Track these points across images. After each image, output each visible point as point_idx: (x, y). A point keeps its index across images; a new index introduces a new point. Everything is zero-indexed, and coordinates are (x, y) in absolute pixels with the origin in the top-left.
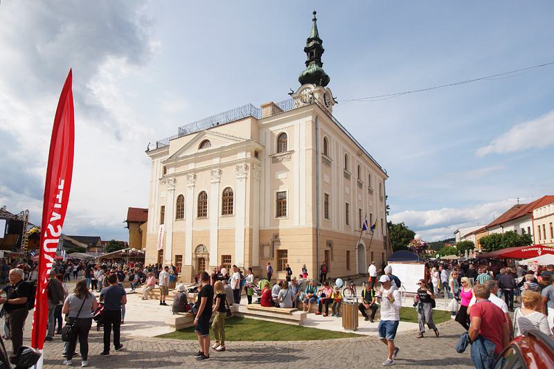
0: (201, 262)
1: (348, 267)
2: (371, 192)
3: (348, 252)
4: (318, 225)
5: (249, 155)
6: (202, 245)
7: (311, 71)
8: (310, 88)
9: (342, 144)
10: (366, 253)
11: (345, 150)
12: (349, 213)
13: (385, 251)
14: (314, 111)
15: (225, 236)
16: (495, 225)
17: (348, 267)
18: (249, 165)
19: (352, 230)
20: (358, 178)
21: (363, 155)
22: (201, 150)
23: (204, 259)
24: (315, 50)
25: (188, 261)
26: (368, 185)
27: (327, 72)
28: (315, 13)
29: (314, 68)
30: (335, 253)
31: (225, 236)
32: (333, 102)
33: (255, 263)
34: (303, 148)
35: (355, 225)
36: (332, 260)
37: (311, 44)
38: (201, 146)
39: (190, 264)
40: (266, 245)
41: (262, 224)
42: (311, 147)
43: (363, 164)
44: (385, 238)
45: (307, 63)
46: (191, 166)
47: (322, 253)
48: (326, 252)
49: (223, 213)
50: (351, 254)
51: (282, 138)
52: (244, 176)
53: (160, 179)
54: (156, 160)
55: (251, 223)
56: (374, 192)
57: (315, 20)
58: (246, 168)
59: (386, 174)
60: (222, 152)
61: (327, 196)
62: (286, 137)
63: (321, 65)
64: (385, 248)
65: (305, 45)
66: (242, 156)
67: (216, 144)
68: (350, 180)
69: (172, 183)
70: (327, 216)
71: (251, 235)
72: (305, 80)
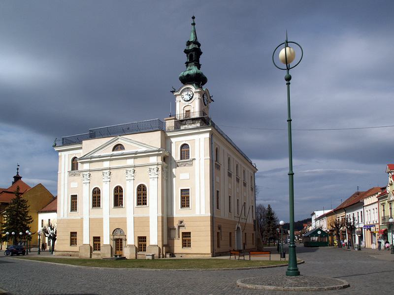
0: (119, 243)
2: (245, 185)
3: (230, 233)
4: (213, 214)
7: (191, 72)
10: (241, 234)
11: (228, 155)
12: (231, 204)
13: (254, 232)
15: (96, 223)
16: (341, 209)
20: (217, 161)
22: (115, 153)
23: (121, 240)
24: (194, 54)
25: (106, 240)
26: (226, 168)
27: (205, 74)
29: (193, 70)
30: (223, 234)
31: (96, 223)
32: (210, 100)
33: (166, 243)
35: (234, 213)
36: (221, 239)
37: (191, 47)
38: (115, 148)
42: (209, 158)
43: (233, 156)
44: (254, 221)
45: (187, 63)
47: (216, 234)
48: (218, 233)
49: (138, 204)
50: (232, 235)
51: (185, 147)
52: (156, 176)
56: (247, 185)
57: (194, 24)
59: (255, 168)
60: (135, 155)
61: (218, 192)
62: (189, 148)
63: (199, 66)
64: (255, 230)
65: (186, 47)
66: (154, 160)
68: (231, 178)
70: (218, 208)
71: (162, 221)
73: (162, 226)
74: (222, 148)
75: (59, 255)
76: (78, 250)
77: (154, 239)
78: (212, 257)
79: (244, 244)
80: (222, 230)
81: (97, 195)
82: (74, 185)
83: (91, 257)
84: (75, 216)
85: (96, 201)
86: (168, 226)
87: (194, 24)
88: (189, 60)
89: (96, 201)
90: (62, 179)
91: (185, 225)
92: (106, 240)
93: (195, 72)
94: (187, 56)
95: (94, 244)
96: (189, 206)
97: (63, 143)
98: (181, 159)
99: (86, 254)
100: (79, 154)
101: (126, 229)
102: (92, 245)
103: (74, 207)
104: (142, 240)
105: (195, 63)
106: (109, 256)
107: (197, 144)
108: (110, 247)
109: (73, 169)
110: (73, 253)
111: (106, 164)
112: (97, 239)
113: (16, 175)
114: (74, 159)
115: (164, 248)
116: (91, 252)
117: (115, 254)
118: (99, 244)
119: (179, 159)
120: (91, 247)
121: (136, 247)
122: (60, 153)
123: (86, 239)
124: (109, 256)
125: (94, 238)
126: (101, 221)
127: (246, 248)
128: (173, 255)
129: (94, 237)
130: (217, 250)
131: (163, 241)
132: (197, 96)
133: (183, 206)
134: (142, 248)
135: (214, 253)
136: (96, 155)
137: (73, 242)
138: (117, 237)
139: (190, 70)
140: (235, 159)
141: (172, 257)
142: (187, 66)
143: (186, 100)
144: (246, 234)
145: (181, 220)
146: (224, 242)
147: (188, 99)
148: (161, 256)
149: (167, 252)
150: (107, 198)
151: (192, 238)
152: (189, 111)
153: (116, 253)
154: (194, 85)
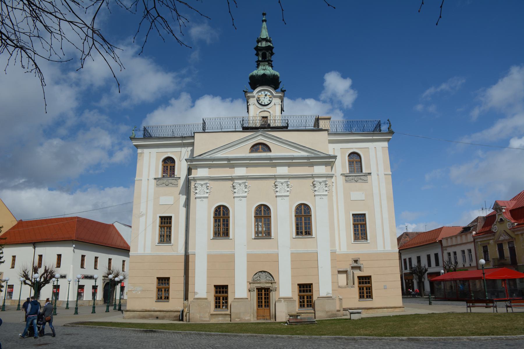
0: (264, 295)
15: (305, 261)
25: (241, 290)
31: (305, 261)
38: (255, 148)
60: (290, 162)
67: (278, 151)
75: (134, 317)
84: (165, 250)
91: (362, 266)
92: (241, 290)
97: (144, 135)
104: (305, 289)
107: (372, 153)
110: (162, 314)
119: (348, 172)
122: (139, 151)
126: (230, 259)
136: (219, 155)
138: (259, 285)
143: (263, 104)
145: (355, 257)
152: (266, 117)
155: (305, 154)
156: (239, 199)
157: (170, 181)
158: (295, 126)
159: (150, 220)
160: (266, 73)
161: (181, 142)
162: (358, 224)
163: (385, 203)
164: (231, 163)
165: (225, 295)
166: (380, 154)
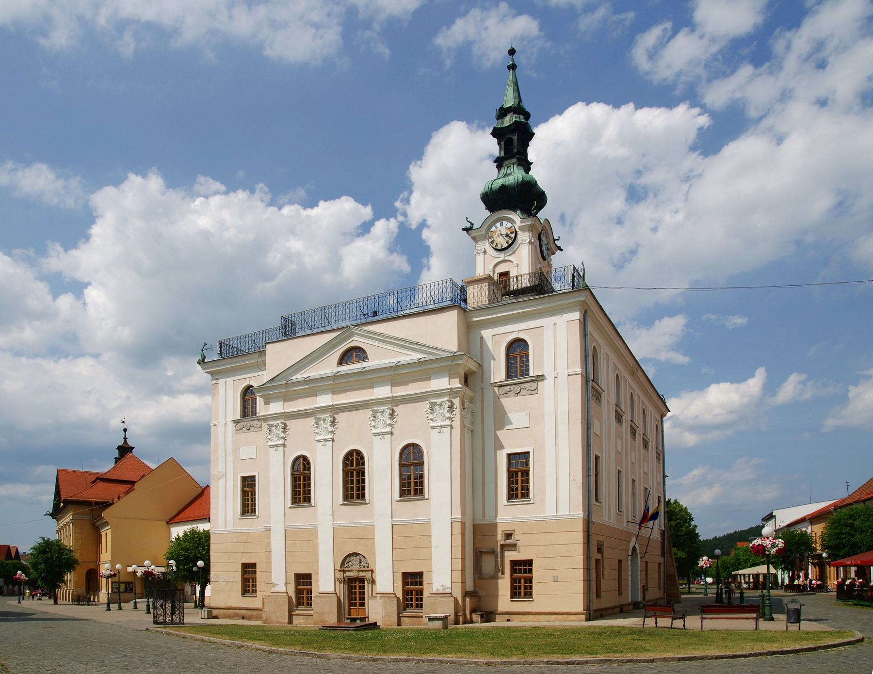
0: (355, 587)
1: (620, 593)
3: (620, 561)
5: (456, 384)
6: (357, 554)
7: (510, 180)
8: (512, 221)
9: (613, 358)
14: (584, 301)
15: (300, 540)
17: (620, 593)
18: (457, 402)
19: (625, 521)
21: (639, 373)
22: (346, 368)
23: (362, 580)
25: (326, 582)
27: (542, 185)
28: (512, 52)
29: (516, 175)
31: (300, 540)
32: (553, 247)
33: (470, 587)
34: (563, 372)
37: (508, 121)
39: (332, 590)
40: (487, 553)
41: (479, 516)
46: (324, 400)
48: (597, 560)
51: (517, 350)
52: (448, 422)
53: (236, 422)
54: (221, 381)
55: (463, 513)
58: (451, 408)
60: (395, 374)
61: (597, 458)
63: (527, 166)
64: (663, 555)
65: (496, 124)
66: (441, 383)
67: (379, 357)
69: (279, 431)
72: (497, 200)
73: (463, 546)
74: (604, 350)
76: (261, 606)
77: (443, 576)
78: (588, 619)
79: (645, 589)
80: (606, 555)
81: (627, 256)
82: (248, 452)
83: (399, 624)
84: (249, 524)
85: (301, 489)
86: (482, 547)
87: (513, 67)
88: (503, 154)
89: (301, 489)
90: (221, 438)
91: (519, 543)
92: (326, 582)
93: (520, 180)
94: (499, 144)
95: (298, 592)
96: (528, 495)
97: (221, 354)
98: (508, 376)
99: (278, 616)
100: (257, 379)
101: (374, 554)
102: (292, 593)
103: (248, 506)
104: (413, 583)
105: (518, 159)
106: (332, 620)
108: (396, 601)
109: (244, 414)
110: (249, 613)
111: (324, 400)
112: (303, 581)
113: (121, 443)
114: (248, 391)
115: (468, 599)
116: (290, 611)
117: (347, 616)
118: (310, 592)
120: (290, 598)
121: (398, 598)
123: (277, 579)
124: (332, 620)
125: (298, 577)
126: (312, 534)
127: (647, 598)
128: (488, 616)
129: (532, 560)
130: (595, 605)
131: (463, 582)
132: (524, 237)
133: (512, 495)
134: (411, 599)
135: (592, 614)
136: (299, 376)
137: (249, 585)
139: (506, 175)
140: (629, 383)
141: (487, 621)
142: (499, 167)
143: (499, 247)
144: (646, 562)
146: (609, 584)
147: (505, 245)
148: (461, 618)
149: (473, 611)
150: (327, 480)
151: (536, 574)
153: (349, 614)
154: (519, 212)
155: (415, 356)
156: (438, 430)
157: (251, 423)
158: (425, 304)
159: (230, 484)
160: (507, 183)
161: (547, 306)
162: (248, 492)
163: (563, 429)
164: (313, 387)
165: (308, 587)
166: (562, 335)
